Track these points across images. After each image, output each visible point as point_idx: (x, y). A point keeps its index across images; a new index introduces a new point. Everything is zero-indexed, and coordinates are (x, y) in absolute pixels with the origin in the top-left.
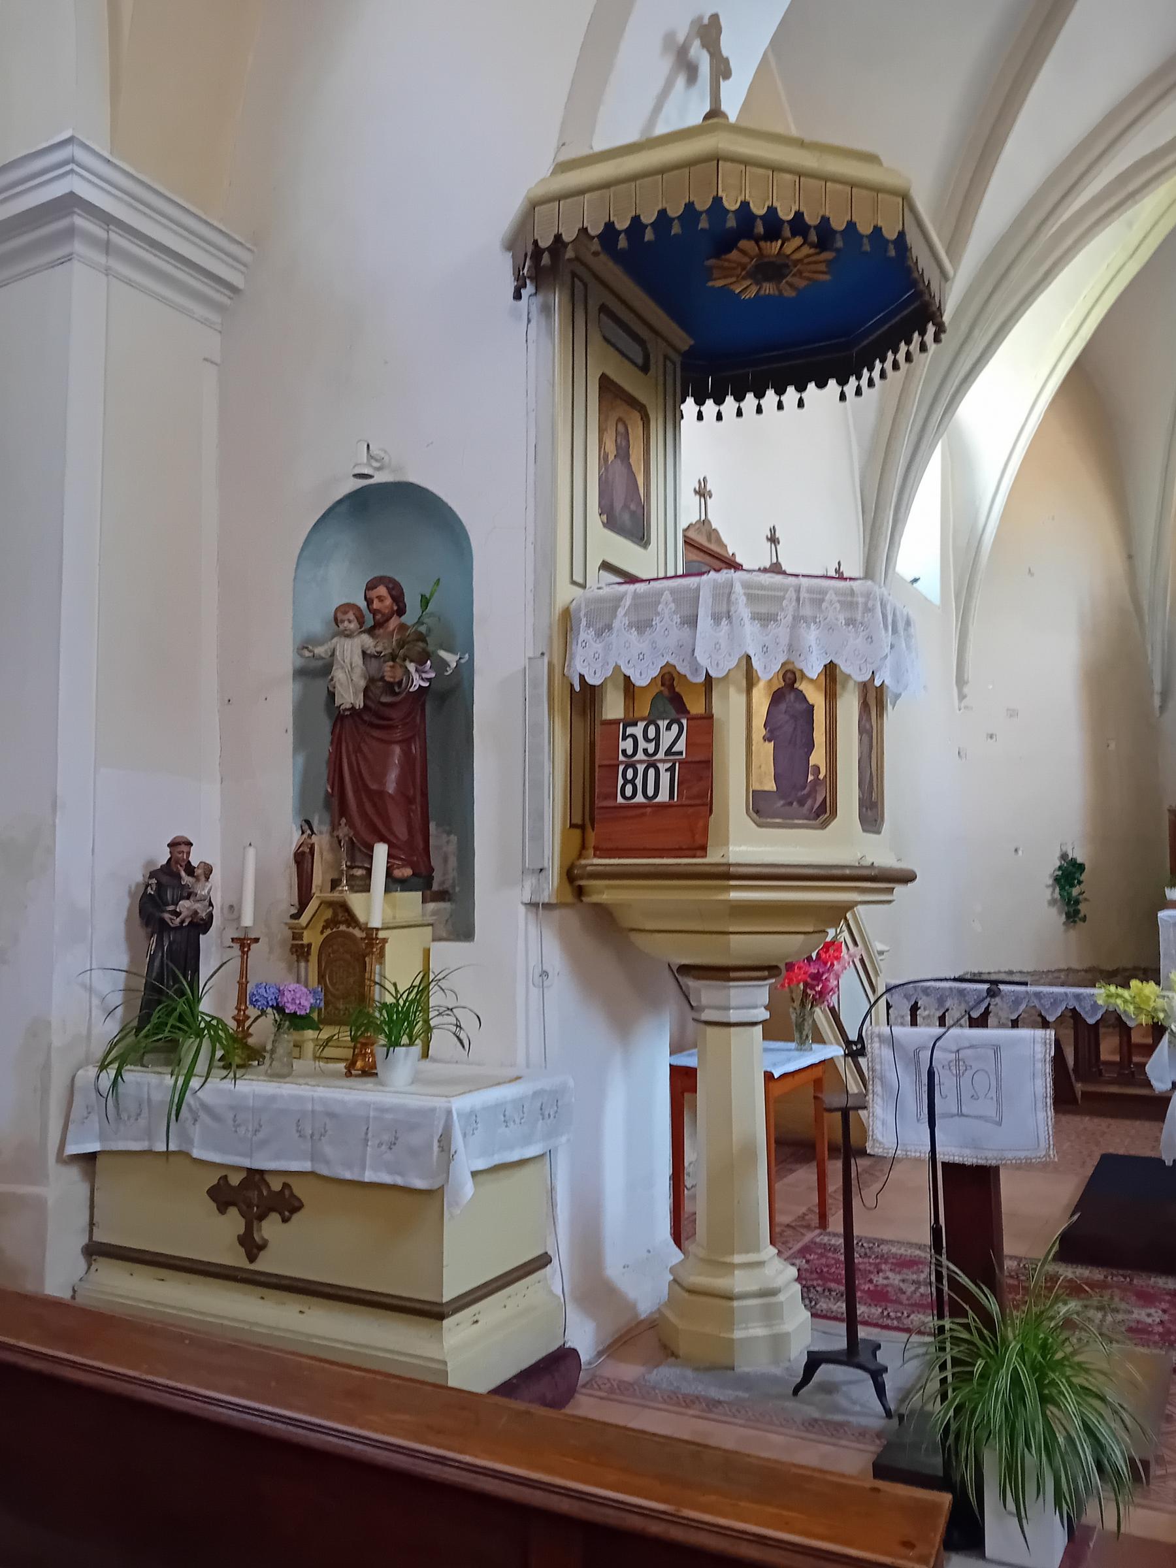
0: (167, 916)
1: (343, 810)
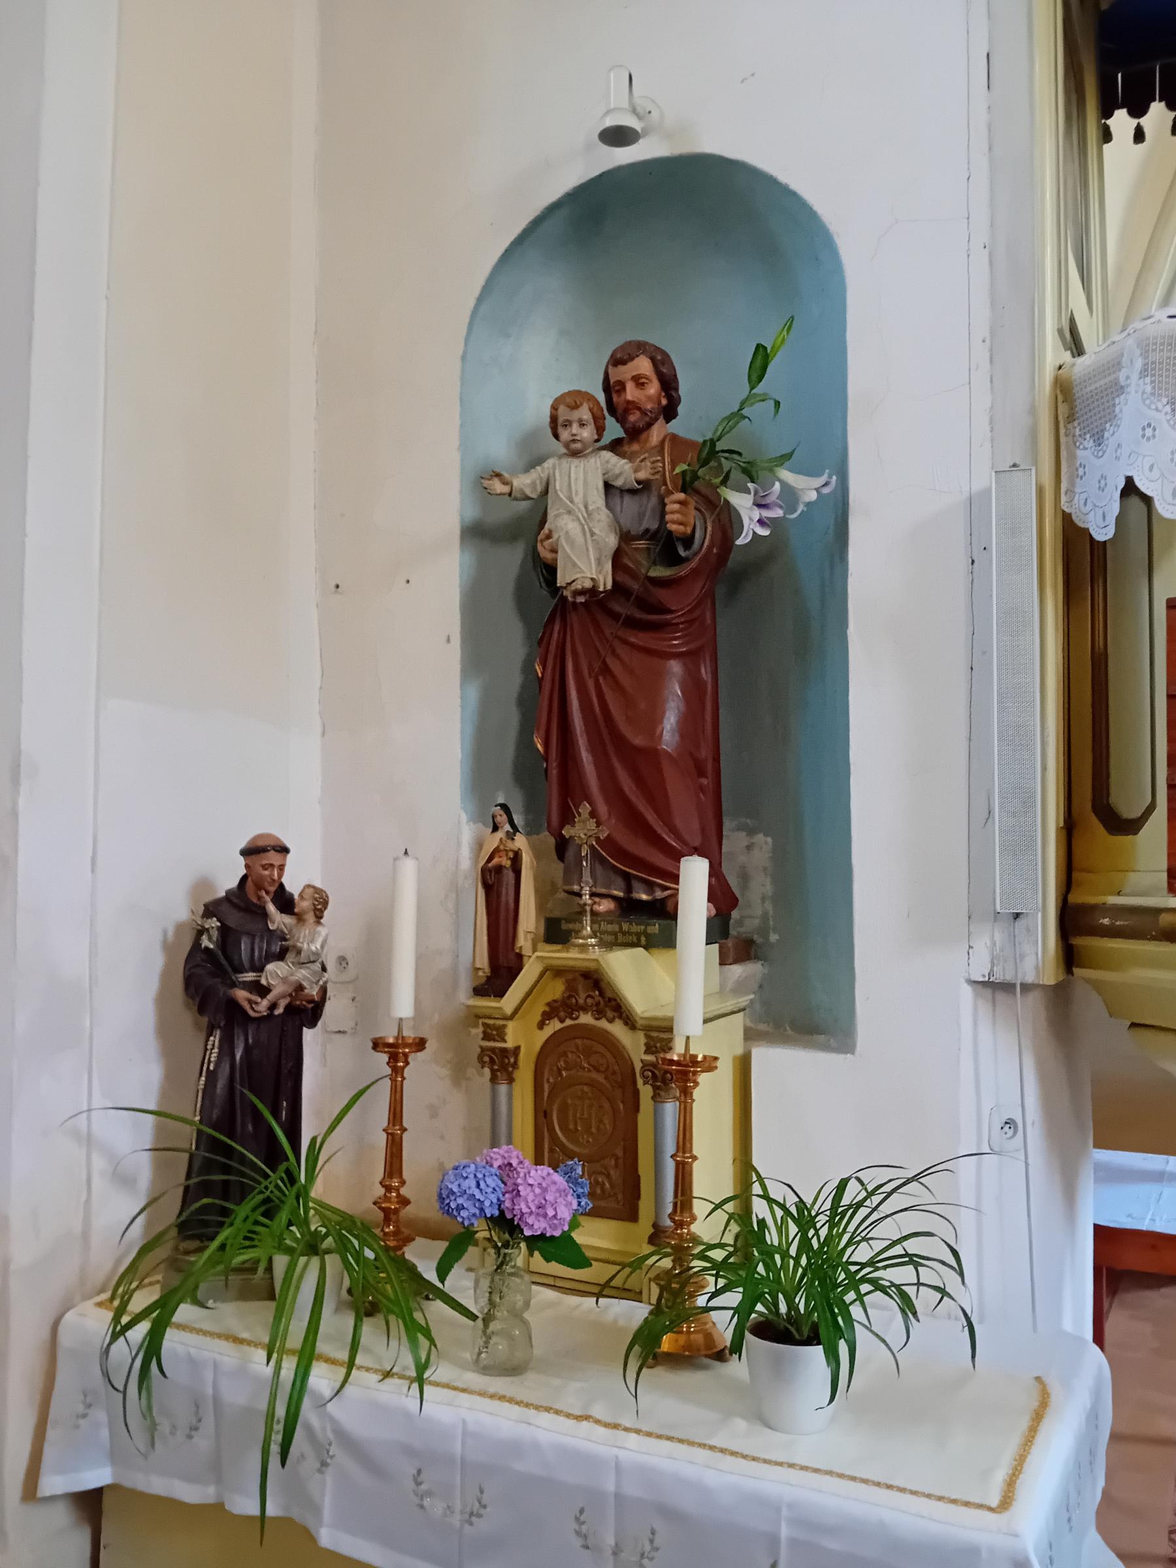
0: (241, 995)
1: (570, 791)
